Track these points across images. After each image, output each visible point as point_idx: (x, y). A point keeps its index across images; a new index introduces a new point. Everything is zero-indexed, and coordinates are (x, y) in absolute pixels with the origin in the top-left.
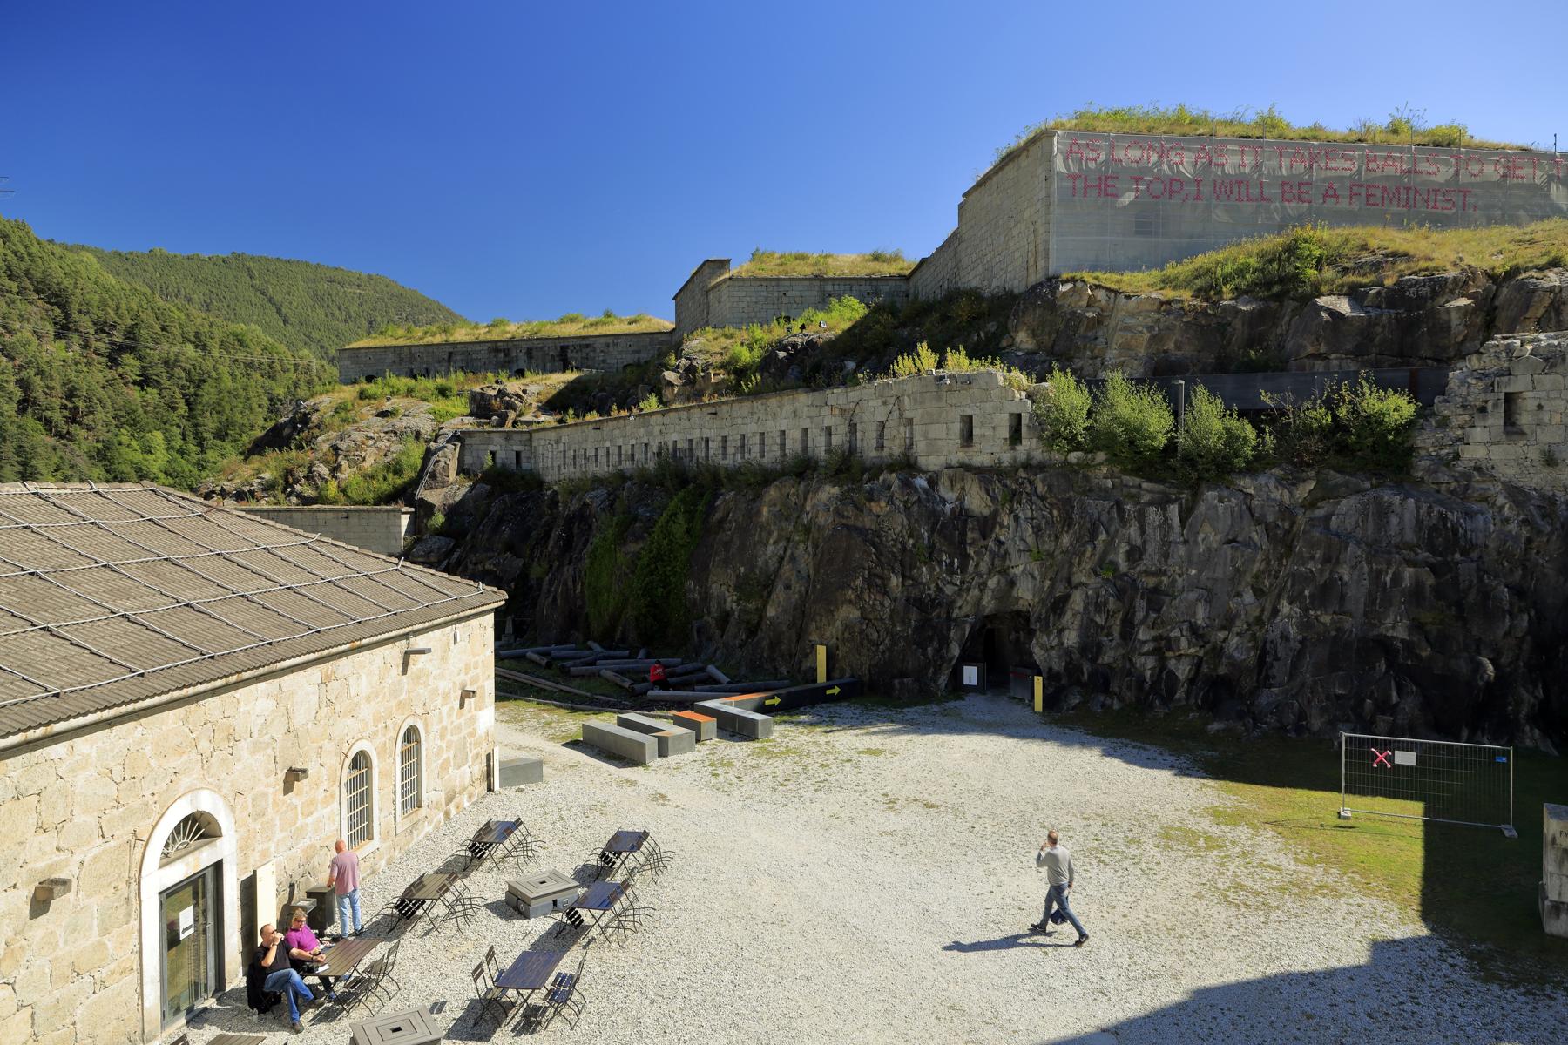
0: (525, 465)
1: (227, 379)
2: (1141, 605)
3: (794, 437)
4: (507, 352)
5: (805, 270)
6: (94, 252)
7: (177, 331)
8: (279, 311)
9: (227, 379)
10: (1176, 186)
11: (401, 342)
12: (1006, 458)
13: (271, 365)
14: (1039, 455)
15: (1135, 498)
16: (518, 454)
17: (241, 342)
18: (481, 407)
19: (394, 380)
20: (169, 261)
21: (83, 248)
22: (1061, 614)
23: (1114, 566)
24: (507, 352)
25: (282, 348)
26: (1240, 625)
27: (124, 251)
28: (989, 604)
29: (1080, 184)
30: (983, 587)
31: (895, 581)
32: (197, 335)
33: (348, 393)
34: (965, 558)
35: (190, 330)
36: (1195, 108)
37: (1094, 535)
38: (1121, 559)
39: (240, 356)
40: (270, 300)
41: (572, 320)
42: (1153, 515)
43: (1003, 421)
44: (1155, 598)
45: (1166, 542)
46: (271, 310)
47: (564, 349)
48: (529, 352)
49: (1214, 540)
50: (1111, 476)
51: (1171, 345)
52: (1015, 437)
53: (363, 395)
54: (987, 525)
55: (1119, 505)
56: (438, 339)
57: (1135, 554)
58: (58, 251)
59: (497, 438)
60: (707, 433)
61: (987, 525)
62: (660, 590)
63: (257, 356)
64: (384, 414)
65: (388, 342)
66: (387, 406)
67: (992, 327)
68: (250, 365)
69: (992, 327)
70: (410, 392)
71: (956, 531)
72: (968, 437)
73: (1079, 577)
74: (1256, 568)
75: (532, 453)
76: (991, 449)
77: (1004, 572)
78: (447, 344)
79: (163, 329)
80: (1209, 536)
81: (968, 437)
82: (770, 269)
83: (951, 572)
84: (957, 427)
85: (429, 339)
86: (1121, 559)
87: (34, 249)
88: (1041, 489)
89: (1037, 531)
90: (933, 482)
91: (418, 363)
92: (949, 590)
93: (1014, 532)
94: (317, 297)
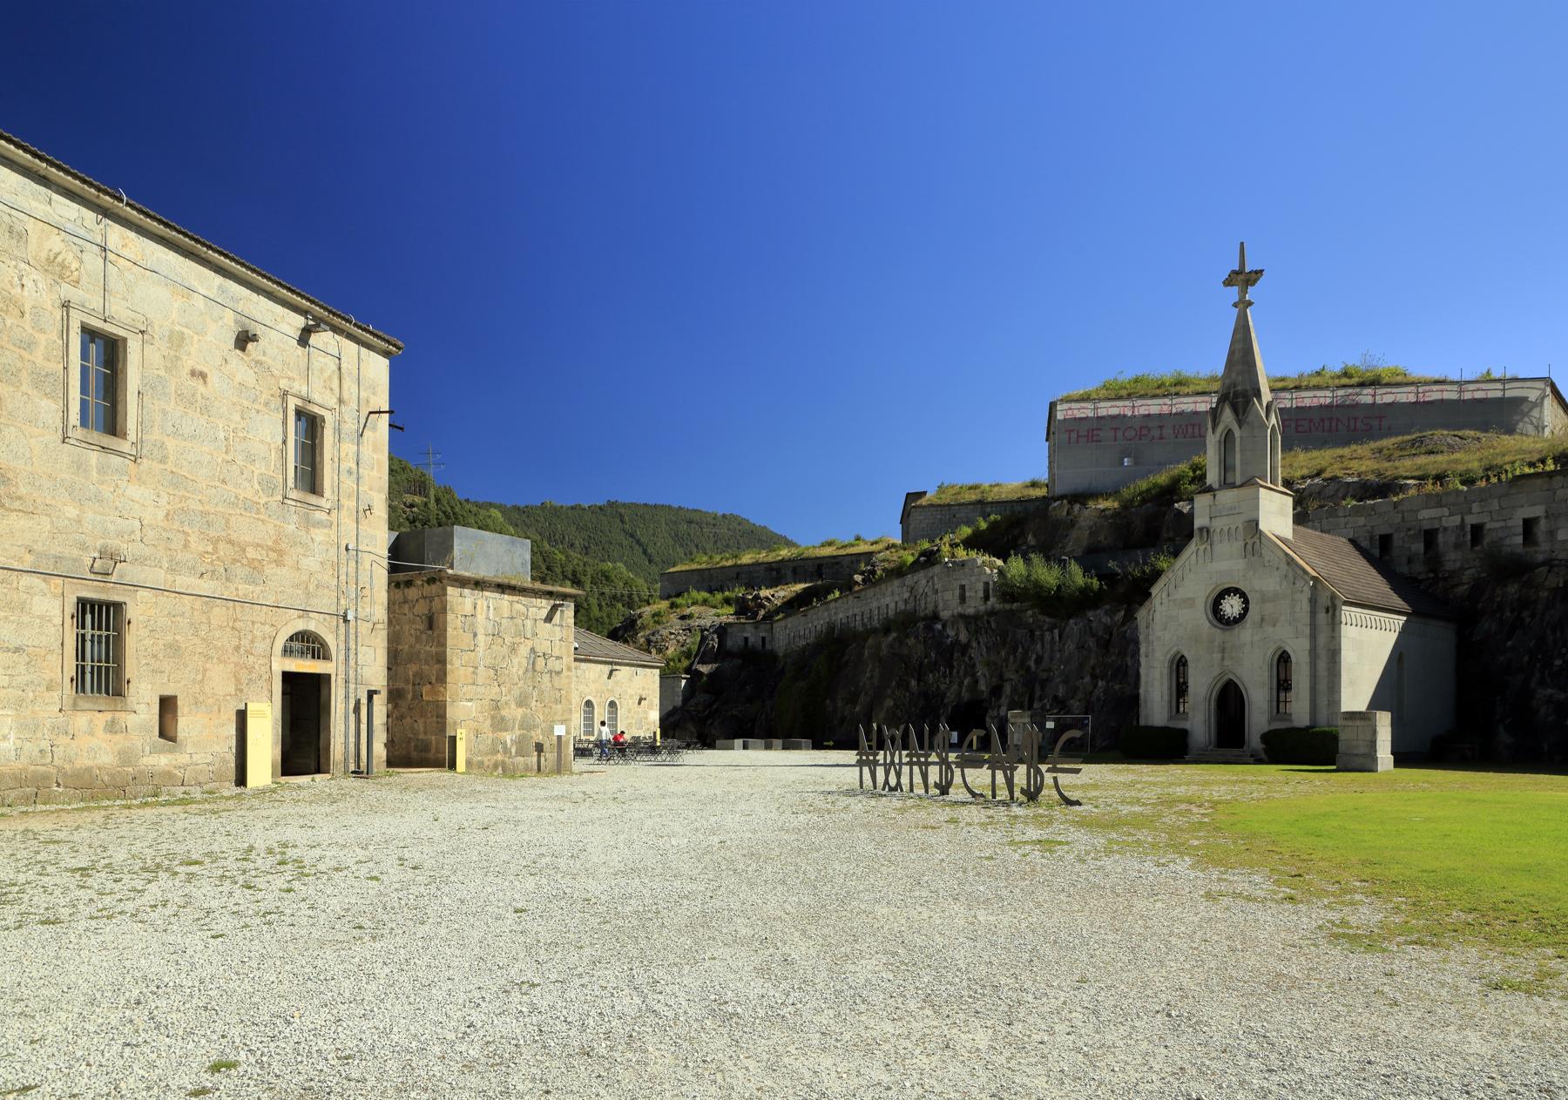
0: (768, 647)
1: (595, 609)
2: (1037, 688)
3: (892, 606)
4: (778, 571)
5: (973, 497)
6: (500, 508)
7: (558, 570)
8: (645, 552)
9: (595, 609)
10: (1144, 432)
11: (704, 566)
12: (982, 608)
13: (630, 596)
14: (998, 606)
15: (1041, 628)
16: (763, 639)
17: (607, 578)
18: (743, 608)
19: (694, 594)
20: (556, 511)
21: (491, 505)
22: (1000, 697)
23: (1029, 668)
24: (778, 571)
25: (640, 581)
26: (1080, 695)
27: (522, 505)
28: (966, 695)
29: (1074, 435)
30: (961, 684)
31: (913, 683)
32: (574, 573)
33: (664, 605)
34: (952, 667)
35: (569, 569)
36: (1387, 360)
37: (1015, 650)
38: (1032, 664)
39: (607, 590)
40: (638, 542)
41: (830, 544)
42: (1048, 637)
43: (980, 586)
44: (1044, 683)
45: (1052, 651)
46: (638, 550)
47: (820, 567)
48: (794, 571)
49: (1072, 647)
50: (1034, 615)
51: (1101, 538)
52: (986, 598)
53: (673, 606)
54: (965, 648)
55: (1032, 632)
56: (730, 563)
57: (1039, 660)
58: (474, 509)
59: (749, 628)
60: (856, 611)
61: (965, 648)
62: (1444, 992)
63: (620, 589)
64: (683, 618)
65: (695, 566)
66: (687, 611)
67: (1016, 532)
68: (614, 597)
69: (1016, 532)
70: (705, 602)
71: (949, 654)
72: (963, 599)
73: (1008, 675)
74: (1092, 662)
75: (773, 639)
76: (974, 605)
77: (974, 675)
78: (735, 566)
79: (548, 568)
80: (1070, 646)
81: (963, 599)
82: (947, 499)
83: (944, 676)
84: (957, 592)
85: (725, 563)
86: (1032, 664)
87: (457, 509)
88: (993, 625)
89: (988, 649)
90: (944, 626)
91: (712, 581)
92: (943, 687)
93: (978, 653)
94: (677, 537)
